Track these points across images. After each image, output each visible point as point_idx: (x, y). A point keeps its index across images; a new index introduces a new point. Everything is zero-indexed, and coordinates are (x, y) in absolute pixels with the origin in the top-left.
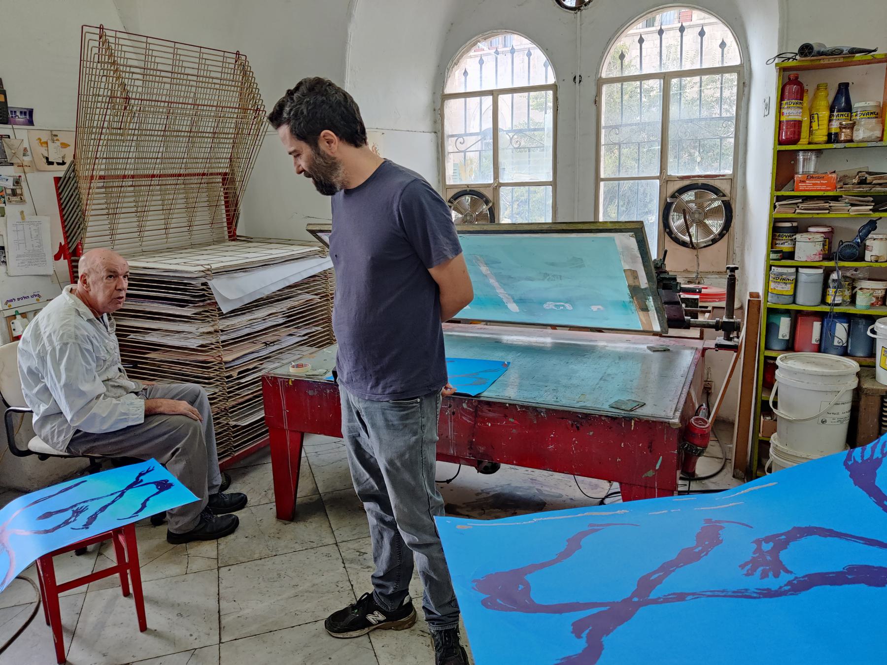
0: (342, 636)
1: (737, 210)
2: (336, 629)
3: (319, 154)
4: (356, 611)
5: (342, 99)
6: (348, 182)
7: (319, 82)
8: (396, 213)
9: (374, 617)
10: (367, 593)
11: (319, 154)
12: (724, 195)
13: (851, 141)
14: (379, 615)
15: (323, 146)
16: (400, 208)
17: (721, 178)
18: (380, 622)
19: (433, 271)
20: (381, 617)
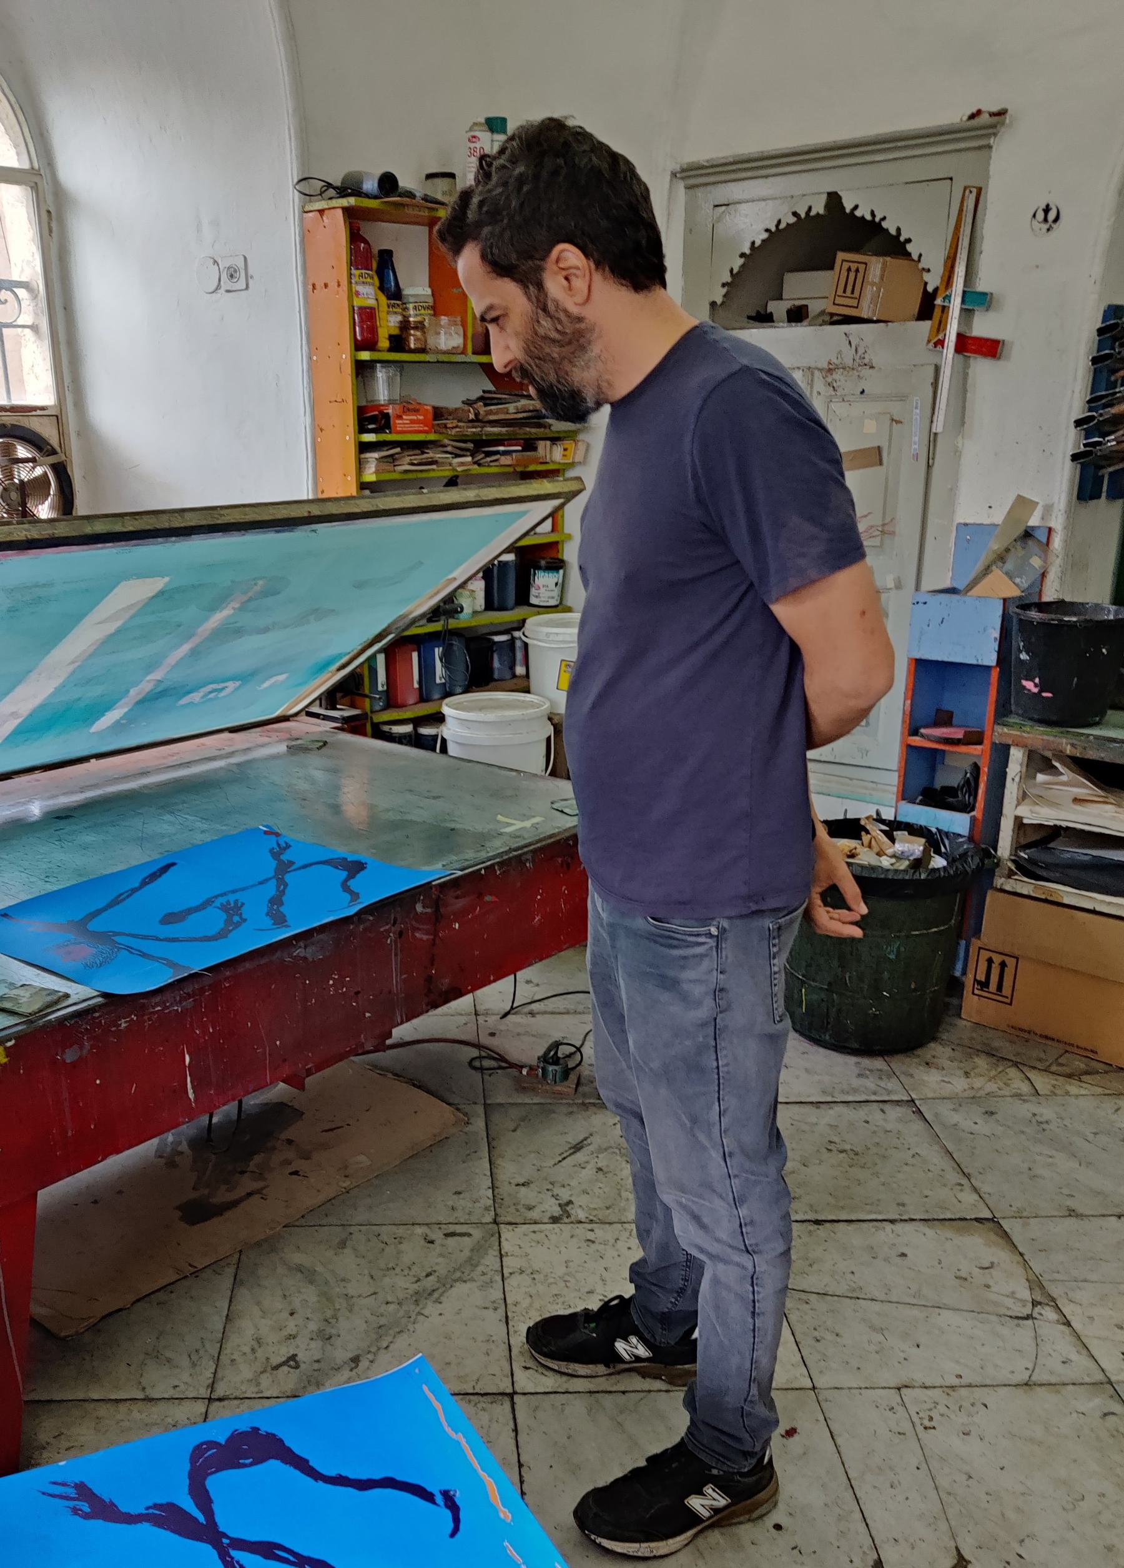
0: (556, 1368)
1: (76, 477)
2: (545, 1350)
3: (545, 309)
4: (593, 1325)
5: (605, 166)
6: (610, 384)
7: (554, 126)
8: (688, 459)
9: (629, 1348)
10: (620, 1297)
11: (545, 309)
12: (53, 452)
13: (423, 350)
14: (640, 1346)
15: (554, 286)
16: (695, 452)
17: (39, 412)
18: (638, 1359)
19: (780, 610)
20: (642, 1351)
